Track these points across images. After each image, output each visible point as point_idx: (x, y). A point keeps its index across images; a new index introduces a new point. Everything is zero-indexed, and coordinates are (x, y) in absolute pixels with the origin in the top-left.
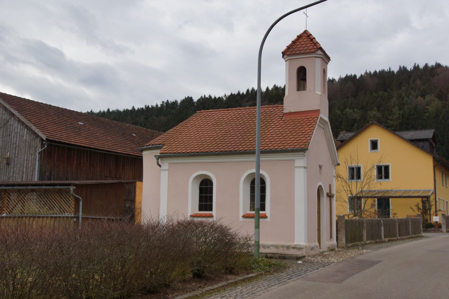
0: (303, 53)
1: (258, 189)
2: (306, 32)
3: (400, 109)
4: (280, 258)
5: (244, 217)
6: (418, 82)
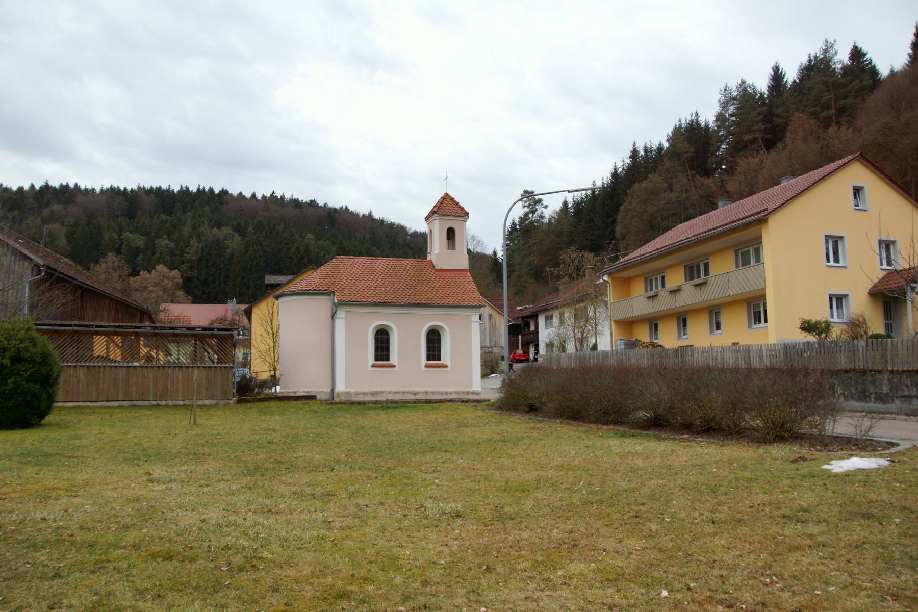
1: (434, 339)
2: (447, 194)
3: (200, 241)
5: (373, 366)
6: (207, 208)
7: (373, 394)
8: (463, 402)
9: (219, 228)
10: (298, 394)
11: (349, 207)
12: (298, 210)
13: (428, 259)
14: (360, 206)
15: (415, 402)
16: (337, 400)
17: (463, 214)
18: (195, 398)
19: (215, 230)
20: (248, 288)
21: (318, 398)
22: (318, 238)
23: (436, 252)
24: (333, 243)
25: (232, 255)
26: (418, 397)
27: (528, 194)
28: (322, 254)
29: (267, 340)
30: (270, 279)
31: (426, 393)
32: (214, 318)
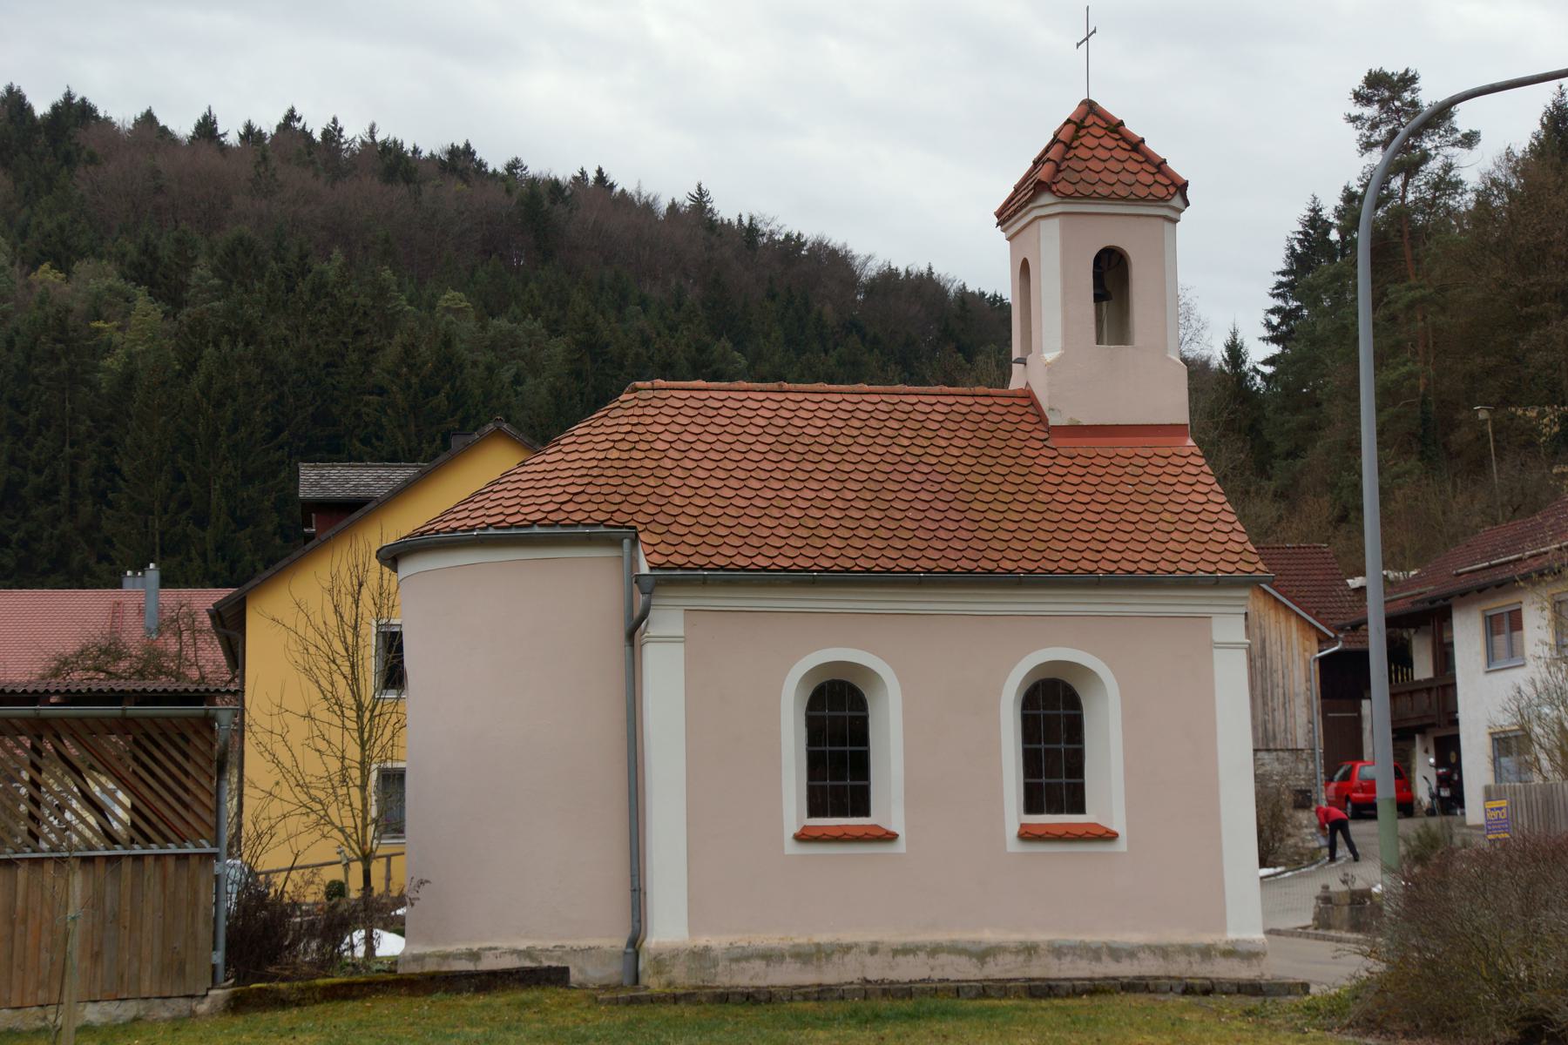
0: (1143, 199)
1: (1053, 724)
2: (1089, 107)
4: (1239, 991)
5: (803, 837)
7: (804, 956)
8: (1188, 990)
9: (63, 264)
10: (488, 964)
11: (613, 176)
12: (401, 190)
13: (1016, 383)
14: (656, 166)
15: (984, 990)
16: (653, 983)
17: (1164, 190)
18: (74, 986)
19: (47, 274)
20: (201, 521)
21: (575, 976)
22: (490, 310)
23: (1050, 356)
24: (554, 329)
25: (128, 379)
26: (994, 970)
27: (1385, 89)
28: (507, 375)
29: (335, 735)
30: (318, 480)
31: (1030, 950)
32: (71, 647)
